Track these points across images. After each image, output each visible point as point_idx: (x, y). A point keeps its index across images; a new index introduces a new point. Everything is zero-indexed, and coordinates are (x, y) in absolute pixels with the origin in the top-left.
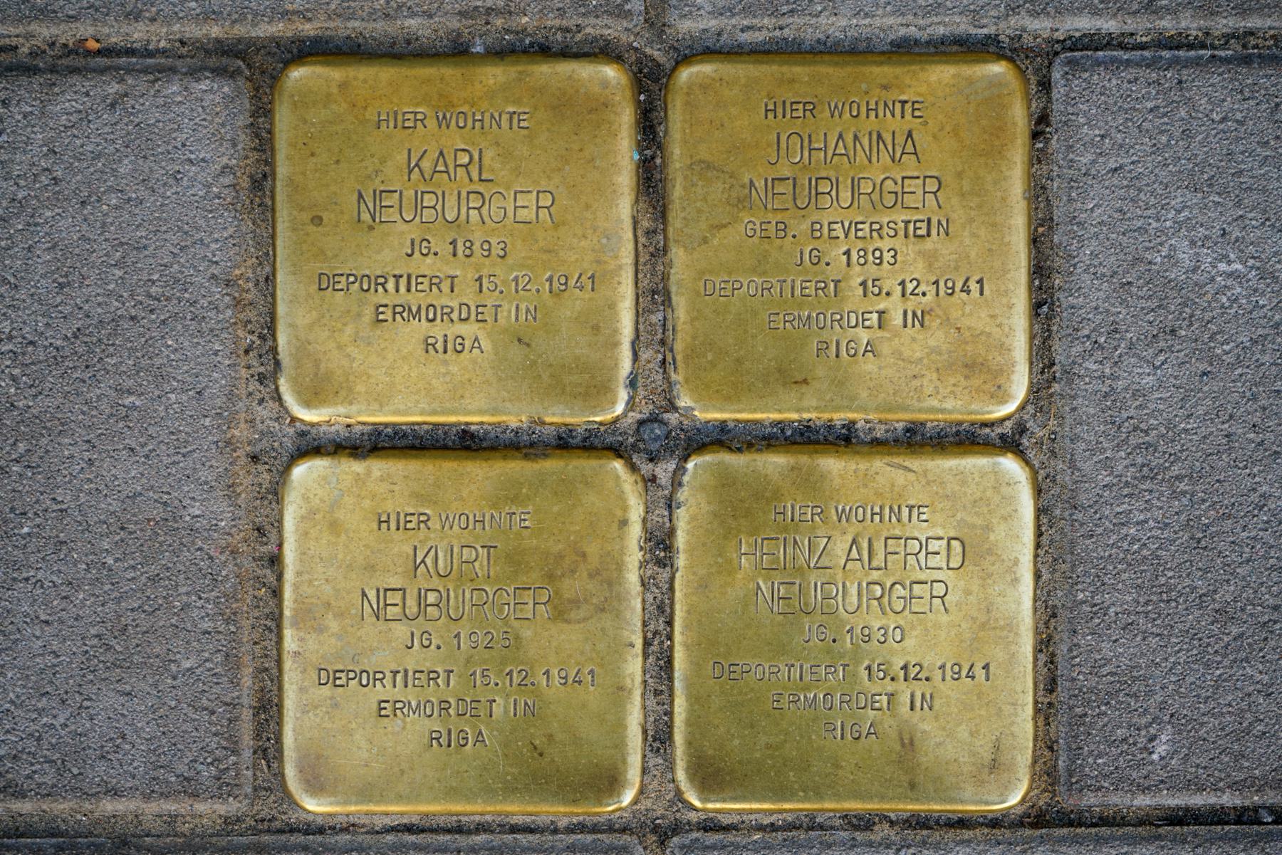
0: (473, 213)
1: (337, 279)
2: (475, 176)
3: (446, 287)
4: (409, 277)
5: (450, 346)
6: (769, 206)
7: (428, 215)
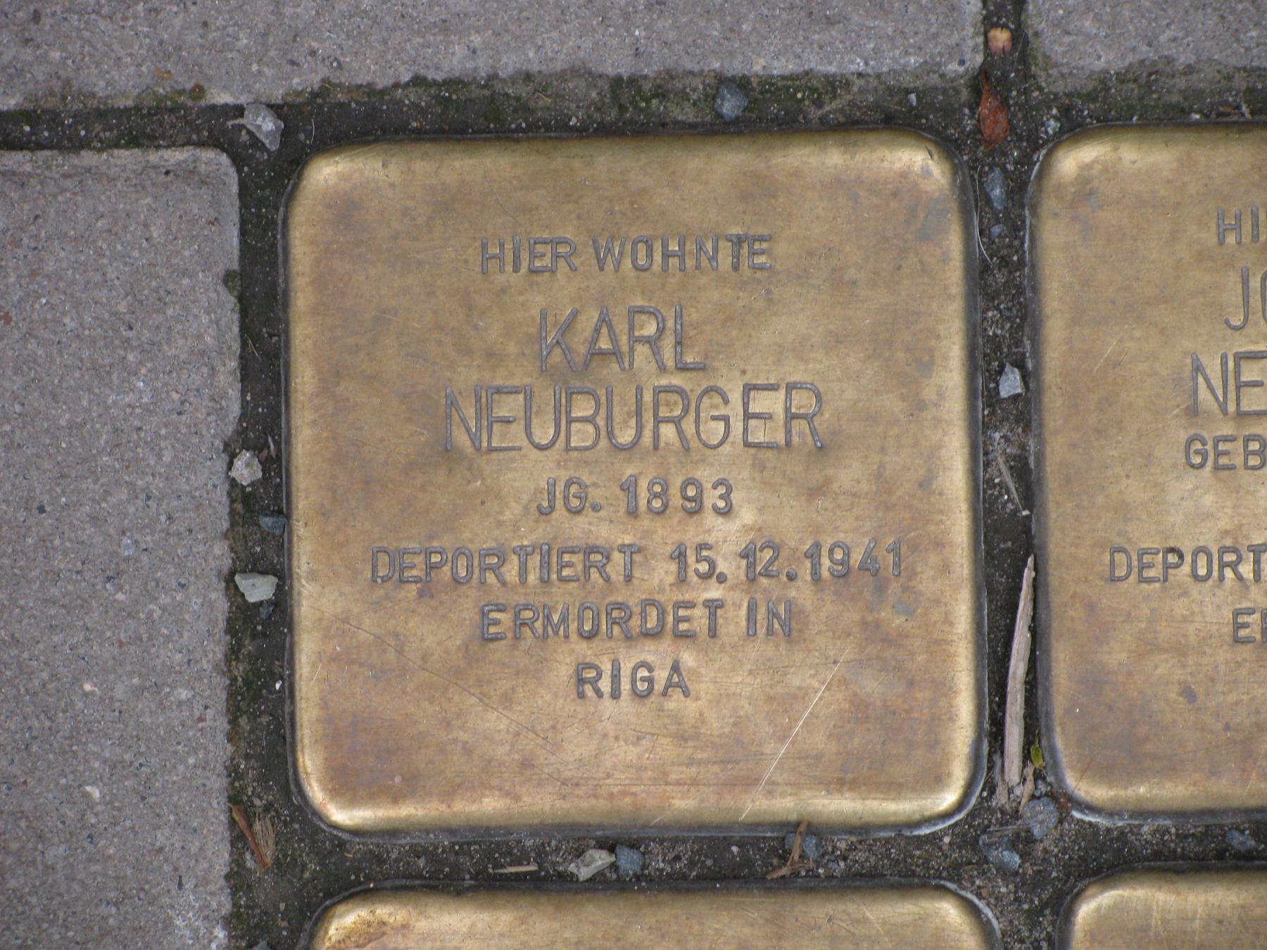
0: (668, 431)
1: (1146, 559)
5: (625, 686)
6: (1232, 408)
7: (582, 435)
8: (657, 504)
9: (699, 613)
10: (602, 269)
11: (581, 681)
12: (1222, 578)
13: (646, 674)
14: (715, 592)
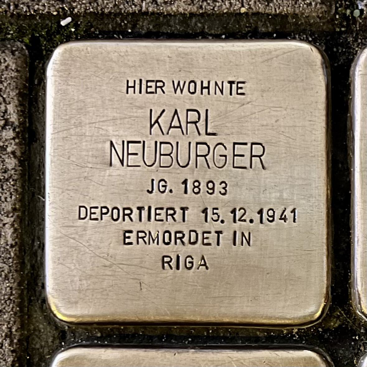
1: (149, 84)
2: (203, 131)
3: (178, 216)
4: (150, 208)
8: (196, 190)
9: (213, 235)
10: (175, 93)
11: (163, 262)
12: (124, 220)
13: (191, 260)
14: (218, 226)
